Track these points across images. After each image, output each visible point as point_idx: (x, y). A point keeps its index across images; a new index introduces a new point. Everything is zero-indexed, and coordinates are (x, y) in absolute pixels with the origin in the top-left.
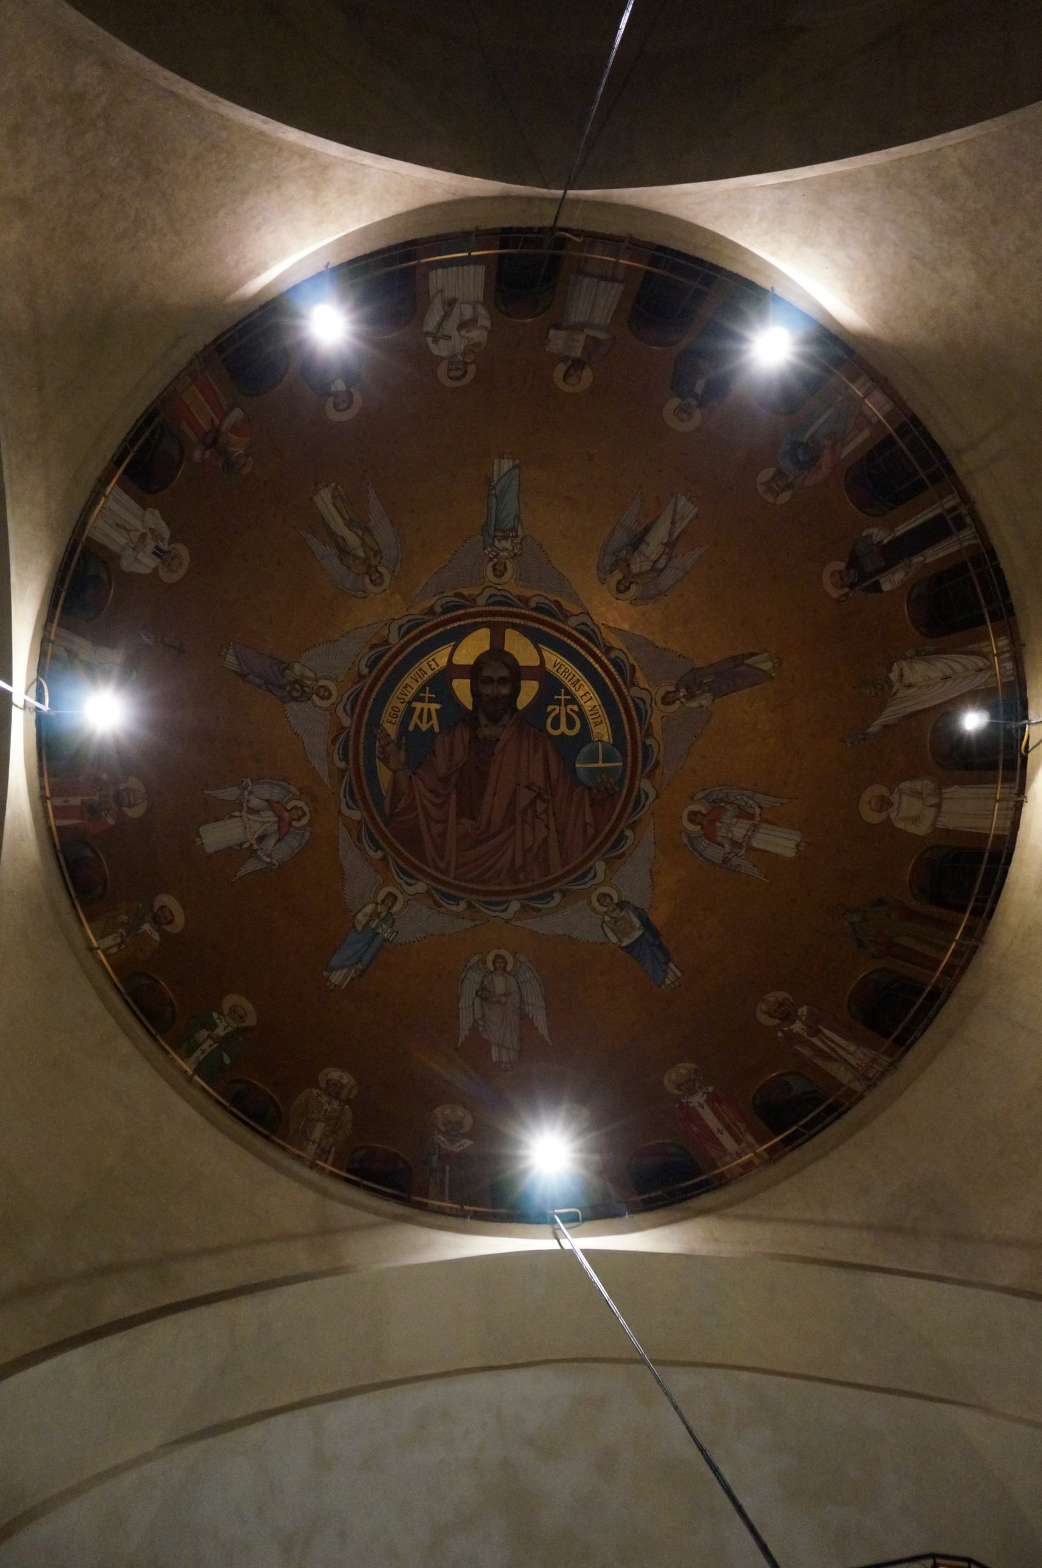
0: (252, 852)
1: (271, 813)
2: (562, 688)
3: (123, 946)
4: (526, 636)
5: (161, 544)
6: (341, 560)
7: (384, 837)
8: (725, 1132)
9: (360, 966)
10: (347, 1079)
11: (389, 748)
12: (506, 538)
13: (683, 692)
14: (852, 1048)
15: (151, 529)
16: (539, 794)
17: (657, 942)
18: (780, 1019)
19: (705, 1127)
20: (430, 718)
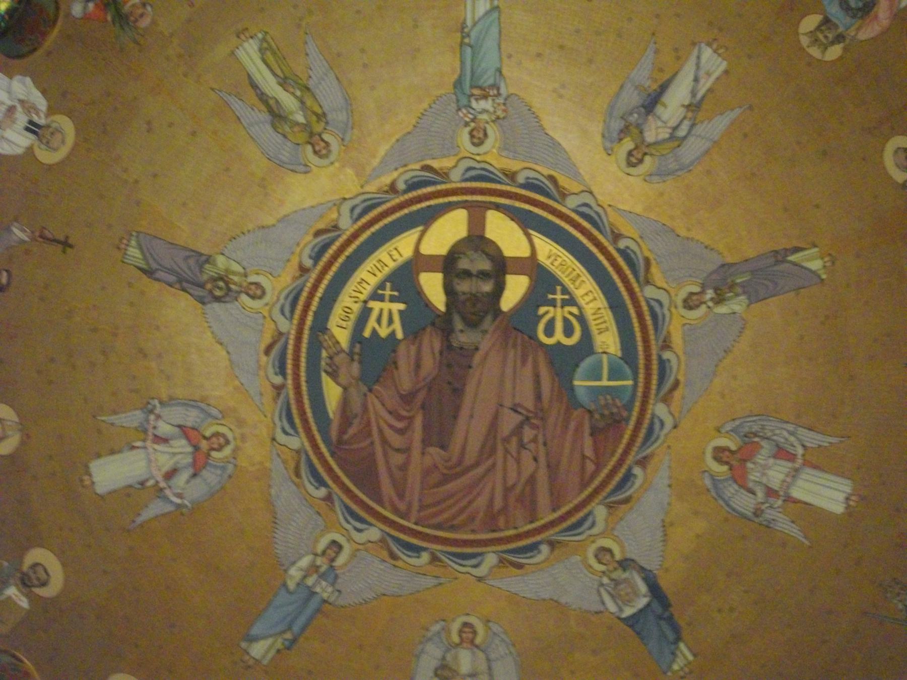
0: (159, 492)
1: (184, 442)
2: (559, 285)
4: (513, 220)
5: (35, 119)
6: (275, 128)
7: (330, 470)
11: (340, 359)
12: (485, 97)
13: (710, 294)
15: (22, 102)
16: (528, 418)
20: (391, 321)
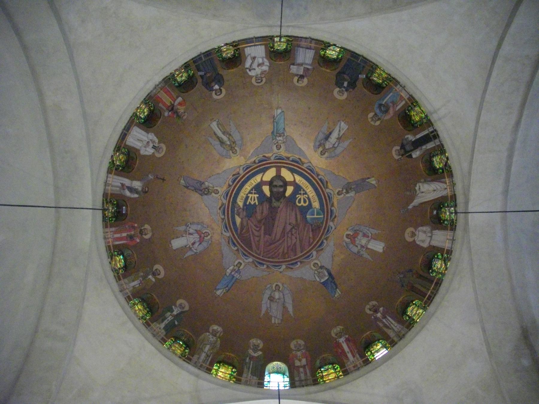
0: (190, 249)
3: (141, 284)
8: (350, 353)
9: (227, 288)
10: (220, 329)
13: (344, 191)
14: (396, 325)
15: (151, 140)
17: (333, 281)
18: (373, 312)
19: (343, 350)
20: (254, 200)
